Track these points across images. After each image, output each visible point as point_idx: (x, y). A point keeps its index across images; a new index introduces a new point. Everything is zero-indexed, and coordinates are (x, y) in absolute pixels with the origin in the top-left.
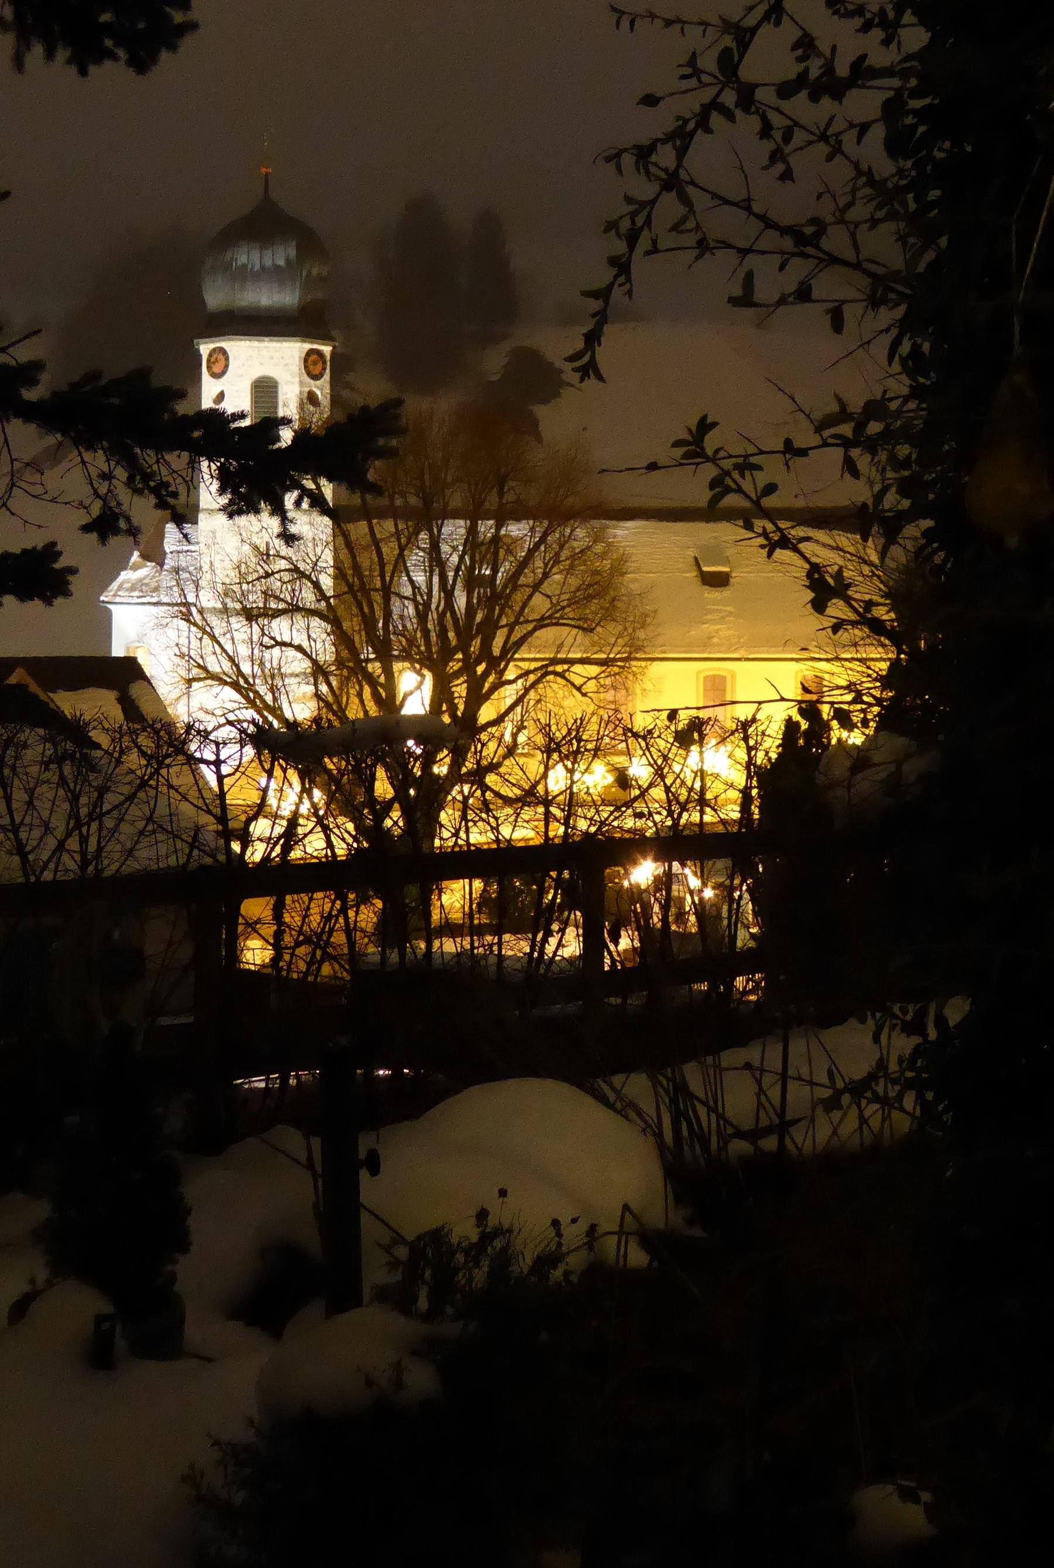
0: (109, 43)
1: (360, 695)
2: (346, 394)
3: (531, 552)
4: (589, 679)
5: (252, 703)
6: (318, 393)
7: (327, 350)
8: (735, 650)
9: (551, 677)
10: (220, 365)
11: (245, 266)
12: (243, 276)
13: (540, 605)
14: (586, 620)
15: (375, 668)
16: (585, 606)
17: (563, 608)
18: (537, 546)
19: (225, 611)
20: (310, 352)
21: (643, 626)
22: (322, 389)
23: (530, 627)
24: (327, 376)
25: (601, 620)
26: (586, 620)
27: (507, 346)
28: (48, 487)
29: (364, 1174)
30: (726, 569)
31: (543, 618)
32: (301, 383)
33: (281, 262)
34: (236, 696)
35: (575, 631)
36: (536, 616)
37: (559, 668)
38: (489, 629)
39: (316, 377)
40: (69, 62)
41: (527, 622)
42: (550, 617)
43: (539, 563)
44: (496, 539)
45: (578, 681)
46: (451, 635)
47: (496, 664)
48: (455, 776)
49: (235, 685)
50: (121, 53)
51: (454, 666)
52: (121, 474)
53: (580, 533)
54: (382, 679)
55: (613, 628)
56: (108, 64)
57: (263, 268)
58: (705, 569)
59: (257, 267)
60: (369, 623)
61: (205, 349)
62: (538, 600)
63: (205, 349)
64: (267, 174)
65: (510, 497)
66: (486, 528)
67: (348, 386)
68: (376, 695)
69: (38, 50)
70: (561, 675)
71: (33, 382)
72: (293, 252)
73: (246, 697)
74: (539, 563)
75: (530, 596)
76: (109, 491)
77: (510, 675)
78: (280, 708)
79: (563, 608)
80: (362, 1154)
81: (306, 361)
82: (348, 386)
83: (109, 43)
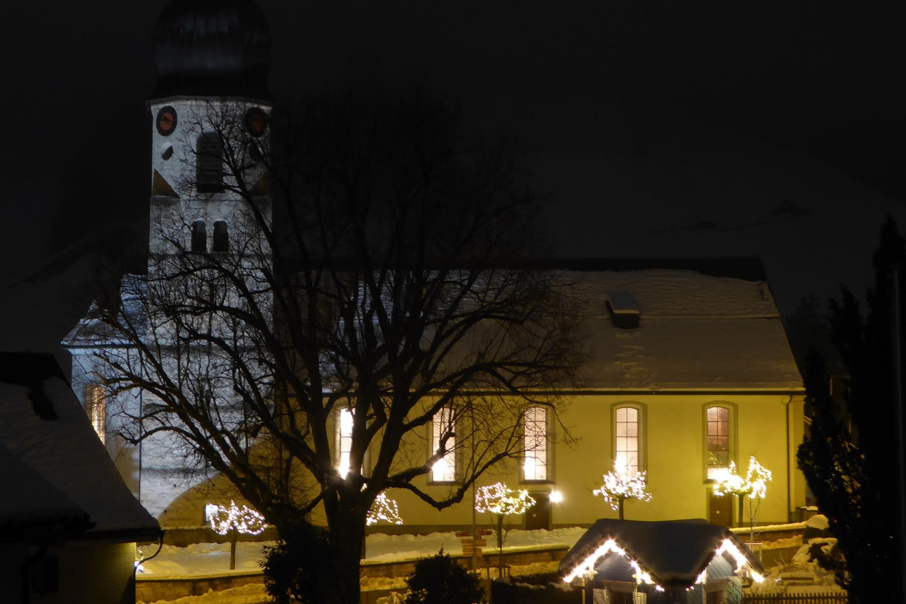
10: (169, 123)
58: (616, 312)
61: (155, 109)
63: (155, 109)
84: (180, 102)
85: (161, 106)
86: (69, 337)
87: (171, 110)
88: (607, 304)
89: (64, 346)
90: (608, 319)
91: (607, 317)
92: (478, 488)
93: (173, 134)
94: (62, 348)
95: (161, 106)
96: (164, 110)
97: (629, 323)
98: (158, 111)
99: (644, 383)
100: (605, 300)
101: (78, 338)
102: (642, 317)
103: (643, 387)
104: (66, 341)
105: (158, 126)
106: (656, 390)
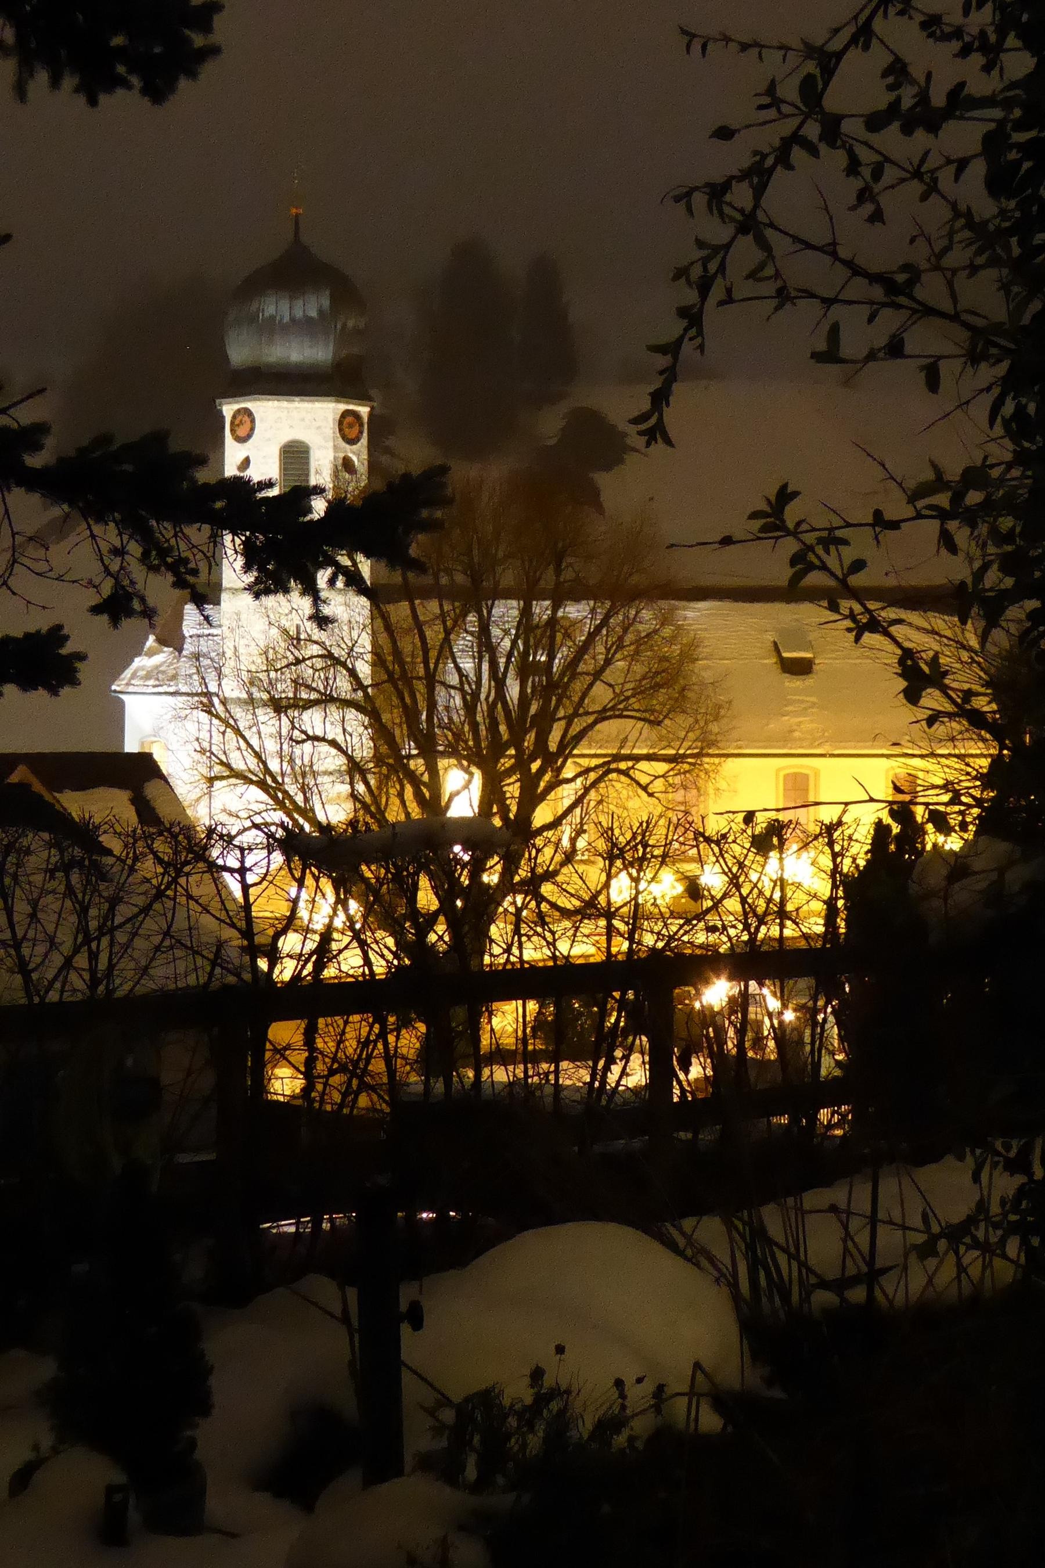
0: (121, 69)
1: (401, 795)
2: (385, 459)
3: (592, 636)
4: (656, 777)
5: (280, 805)
6: (355, 459)
7: (364, 410)
8: (819, 745)
9: (614, 775)
11: (272, 318)
12: (271, 328)
13: (601, 695)
14: (653, 711)
15: (418, 765)
16: (652, 696)
17: (627, 698)
18: (598, 629)
19: (251, 701)
20: (346, 414)
21: (717, 718)
22: (359, 454)
23: (590, 719)
24: (364, 440)
25: (669, 712)
26: (653, 711)
27: (564, 407)
28: (54, 564)
29: (405, 1329)
30: (809, 655)
31: (605, 710)
32: (336, 448)
33: (313, 314)
34: (263, 797)
35: (640, 724)
36: (598, 707)
37: (623, 765)
38: (544, 722)
39: (352, 442)
40: (77, 90)
41: (587, 713)
42: (613, 708)
43: (600, 648)
44: (553, 622)
45: (644, 780)
46: (503, 728)
47: (553, 760)
48: (507, 886)
49: (262, 785)
50: (135, 80)
51: (506, 763)
52: (135, 549)
53: (646, 614)
54: (426, 778)
55: (683, 721)
56: (120, 92)
57: (293, 320)
58: (785, 655)
59: (286, 319)
60: (411, 715)
61: (228, 410)
62: (599, 688)
63: (228, 410)
64: (297, 215)
65: (568, 575)
66: (542, 609)
67: (388, 451)
68: (418, 796)
69: (42, 77)
70: (625, 773)
71: (37, 447)
72: (326, 302)
73: (275, 798)
74: (600, 648)
75: (591, 685)
76: (122, 568)
77: (568, 772)
78: (312, 810)
79: (627, 698)
80: (404, 1307)
81: (340, 423)
82: (388, 451)
83: (121, 69)
84: (258, 403)
85: (236, 407)
86: (123, 679)
87: (248, 413)
88: (775, 644)
89: (115, 691)
90: (776, 663)
91: (774, 660)
92: (1030, 41)
93: (251, 441)
94: (113, 694)
95: (236, 407)
96: (239, 411)
97: (800, 668)
98: (232, 413)
99: (817, 743)
100: (772, 639)
101: (133, 682)
102: (817, 662)
103: (815, 747)
104: (118, 686)
105: (233, 431)
106: (830, 752)
